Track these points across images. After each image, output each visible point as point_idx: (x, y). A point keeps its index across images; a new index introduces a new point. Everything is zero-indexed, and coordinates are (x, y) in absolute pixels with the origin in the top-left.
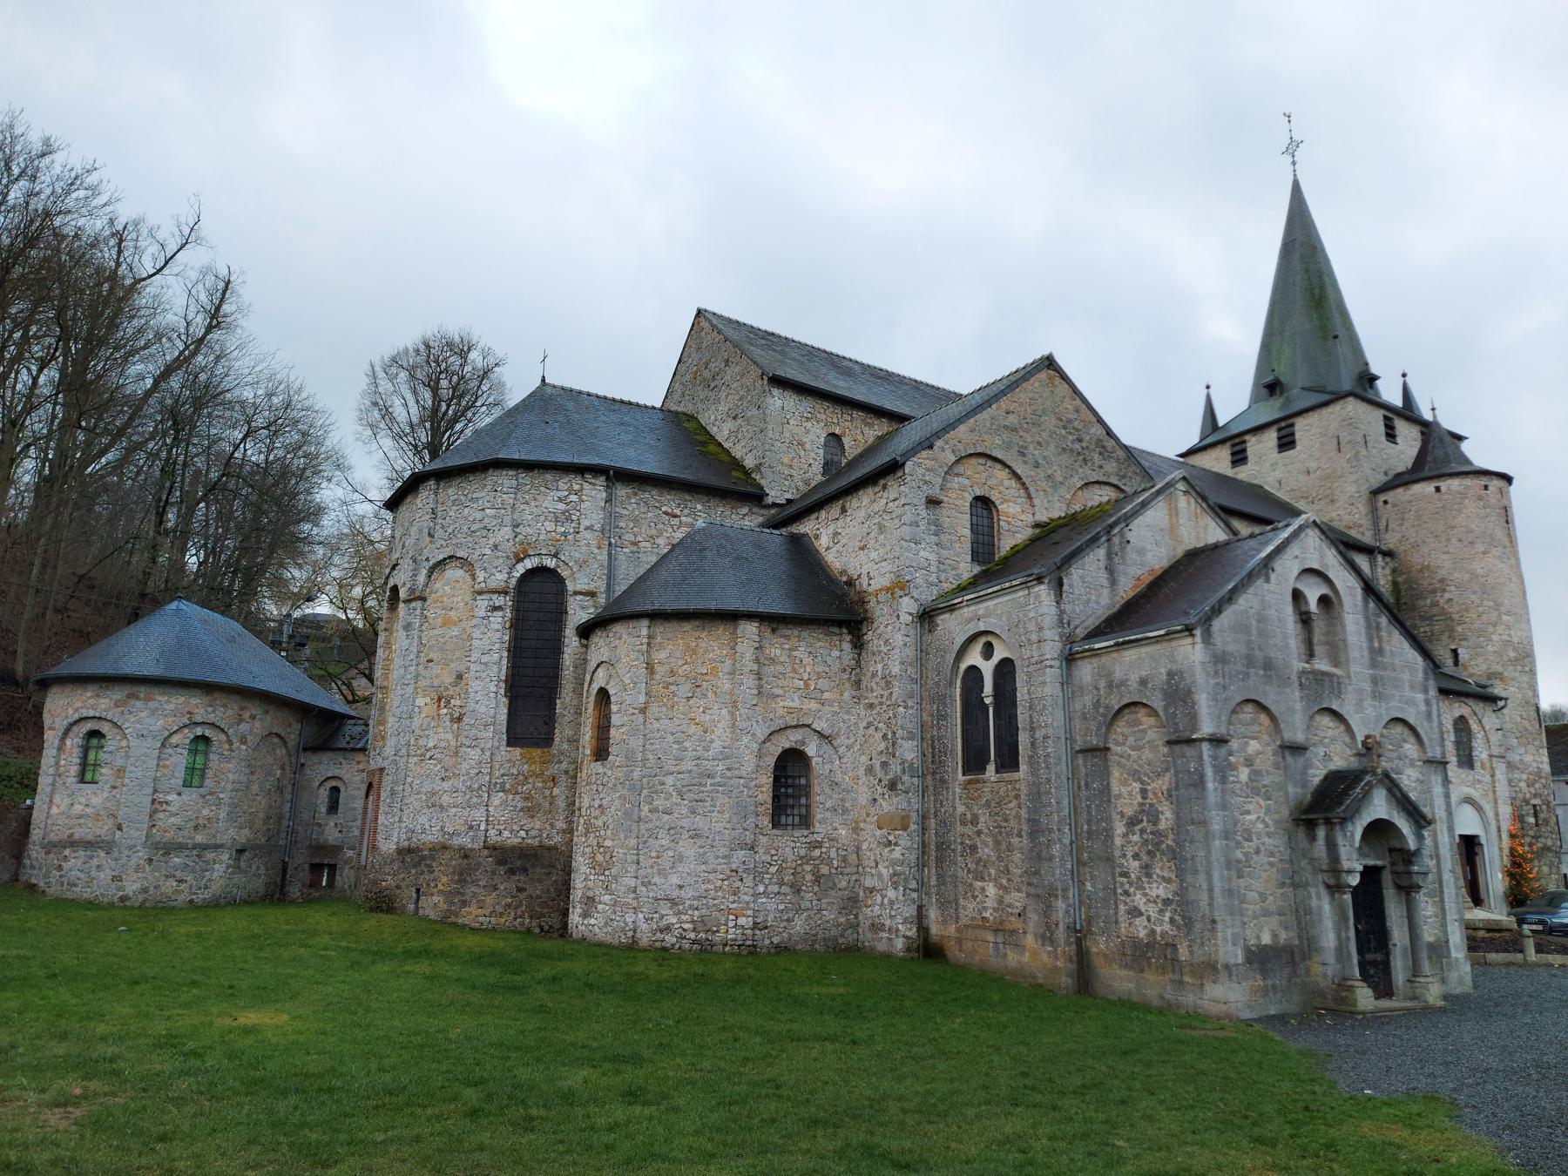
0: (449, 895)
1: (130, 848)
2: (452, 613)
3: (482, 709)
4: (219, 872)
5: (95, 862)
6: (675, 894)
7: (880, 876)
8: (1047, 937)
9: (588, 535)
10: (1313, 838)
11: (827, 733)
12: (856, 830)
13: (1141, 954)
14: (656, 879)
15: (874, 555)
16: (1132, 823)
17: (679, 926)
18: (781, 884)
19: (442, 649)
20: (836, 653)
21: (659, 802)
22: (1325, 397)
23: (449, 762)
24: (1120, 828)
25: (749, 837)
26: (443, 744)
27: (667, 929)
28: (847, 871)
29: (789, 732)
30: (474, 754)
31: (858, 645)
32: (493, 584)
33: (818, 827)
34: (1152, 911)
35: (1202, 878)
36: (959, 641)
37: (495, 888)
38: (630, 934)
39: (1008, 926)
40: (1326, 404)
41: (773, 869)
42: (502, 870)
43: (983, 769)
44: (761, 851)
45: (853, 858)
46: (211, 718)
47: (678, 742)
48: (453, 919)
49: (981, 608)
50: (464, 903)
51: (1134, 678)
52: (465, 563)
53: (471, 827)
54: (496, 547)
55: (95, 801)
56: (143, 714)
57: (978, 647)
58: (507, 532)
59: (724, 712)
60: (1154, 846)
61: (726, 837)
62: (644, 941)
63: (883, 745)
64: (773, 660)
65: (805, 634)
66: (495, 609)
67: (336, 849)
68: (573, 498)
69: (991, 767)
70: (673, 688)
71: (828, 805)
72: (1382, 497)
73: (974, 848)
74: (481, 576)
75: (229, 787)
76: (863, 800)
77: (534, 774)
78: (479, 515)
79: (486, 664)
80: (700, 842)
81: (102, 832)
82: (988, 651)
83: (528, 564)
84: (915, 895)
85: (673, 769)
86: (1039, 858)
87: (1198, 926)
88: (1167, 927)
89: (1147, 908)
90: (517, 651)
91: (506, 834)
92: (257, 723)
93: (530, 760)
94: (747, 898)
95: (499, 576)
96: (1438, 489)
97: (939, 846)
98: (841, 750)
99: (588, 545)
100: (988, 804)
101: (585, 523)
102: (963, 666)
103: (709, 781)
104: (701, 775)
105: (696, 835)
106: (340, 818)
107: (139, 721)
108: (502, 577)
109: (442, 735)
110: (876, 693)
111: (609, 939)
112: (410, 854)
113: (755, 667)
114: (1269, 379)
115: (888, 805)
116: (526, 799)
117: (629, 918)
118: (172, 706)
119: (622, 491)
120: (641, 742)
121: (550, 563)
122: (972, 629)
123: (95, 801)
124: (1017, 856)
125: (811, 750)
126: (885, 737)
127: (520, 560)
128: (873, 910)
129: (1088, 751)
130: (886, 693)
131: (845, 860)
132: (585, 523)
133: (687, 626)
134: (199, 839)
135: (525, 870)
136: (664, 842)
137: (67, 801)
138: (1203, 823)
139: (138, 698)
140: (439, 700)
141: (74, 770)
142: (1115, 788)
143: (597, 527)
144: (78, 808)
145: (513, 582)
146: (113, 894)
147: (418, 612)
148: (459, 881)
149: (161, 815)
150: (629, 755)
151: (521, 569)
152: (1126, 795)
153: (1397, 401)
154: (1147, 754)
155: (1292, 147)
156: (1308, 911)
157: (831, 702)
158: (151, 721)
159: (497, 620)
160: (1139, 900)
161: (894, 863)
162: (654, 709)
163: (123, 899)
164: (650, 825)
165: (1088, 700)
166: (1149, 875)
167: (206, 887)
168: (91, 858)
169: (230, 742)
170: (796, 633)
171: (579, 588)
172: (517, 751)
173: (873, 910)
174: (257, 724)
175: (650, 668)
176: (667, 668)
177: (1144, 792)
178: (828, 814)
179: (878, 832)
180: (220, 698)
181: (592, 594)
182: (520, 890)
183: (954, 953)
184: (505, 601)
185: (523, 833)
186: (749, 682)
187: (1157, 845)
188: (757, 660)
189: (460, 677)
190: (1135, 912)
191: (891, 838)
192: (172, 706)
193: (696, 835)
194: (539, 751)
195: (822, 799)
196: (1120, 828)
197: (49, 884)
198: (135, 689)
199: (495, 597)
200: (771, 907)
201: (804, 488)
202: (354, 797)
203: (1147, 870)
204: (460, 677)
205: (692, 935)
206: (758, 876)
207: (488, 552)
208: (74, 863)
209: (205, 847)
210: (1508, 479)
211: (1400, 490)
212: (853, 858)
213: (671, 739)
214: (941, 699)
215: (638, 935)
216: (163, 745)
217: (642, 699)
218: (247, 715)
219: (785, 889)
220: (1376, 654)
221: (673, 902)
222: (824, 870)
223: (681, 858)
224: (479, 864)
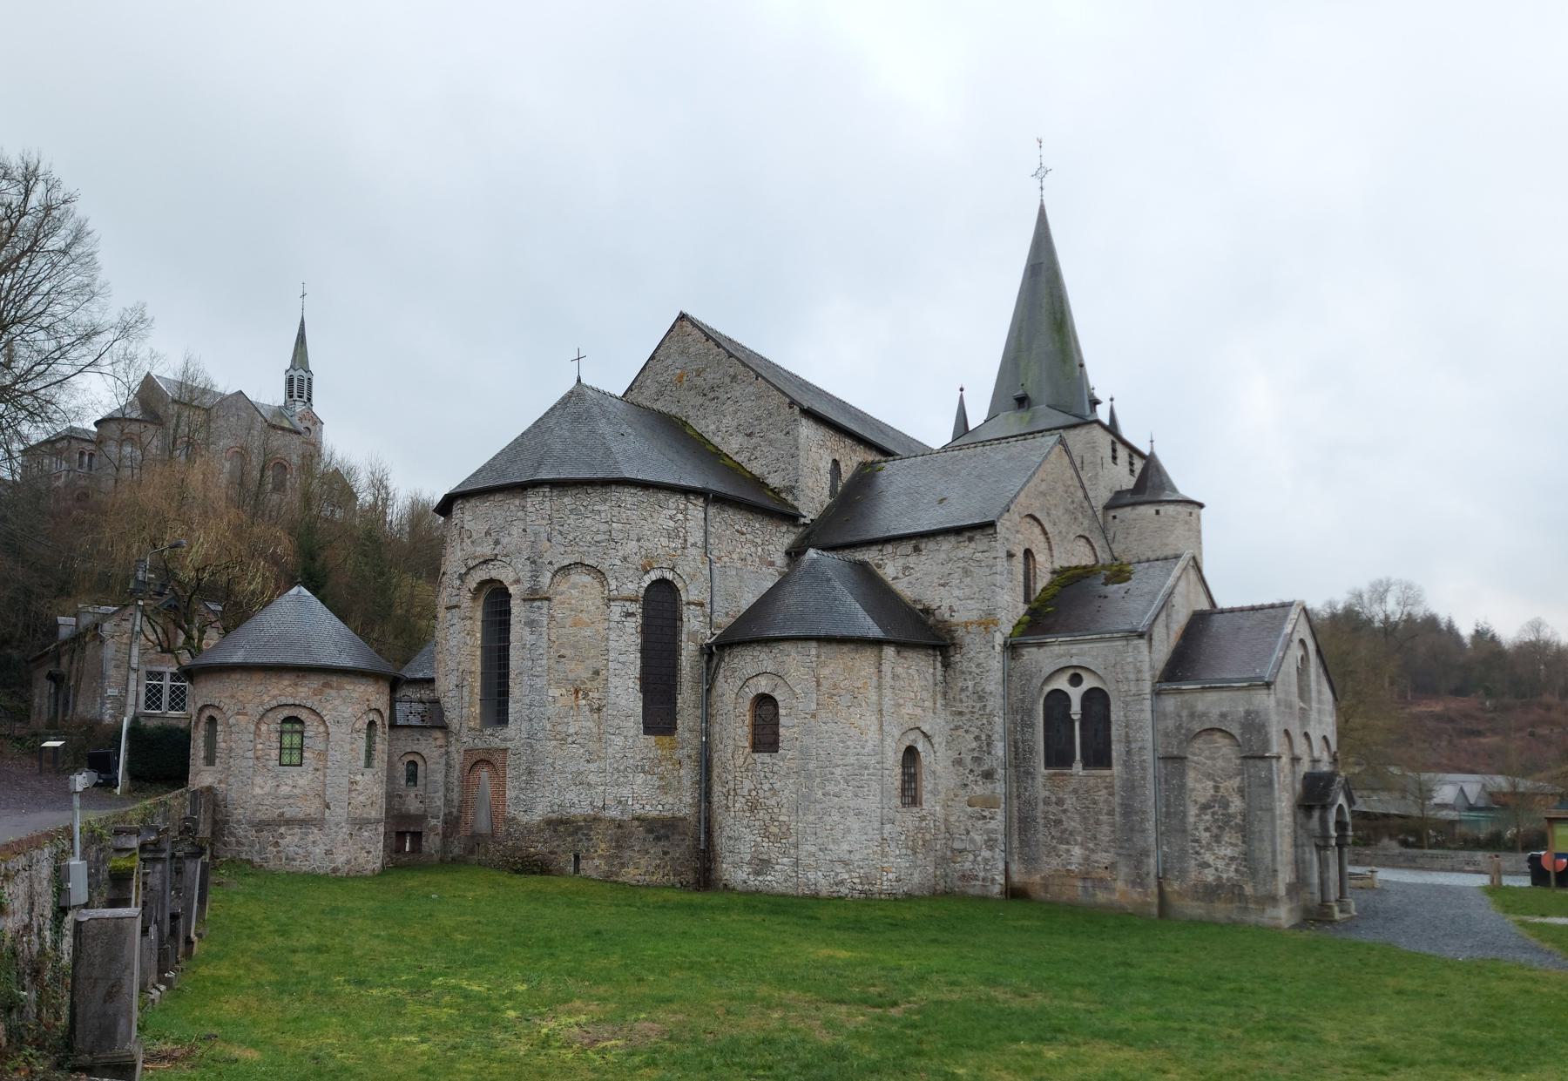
0: (609, 859)
1: (337, 824)
3: (623, 702)
8: (1138, 881)
9: (693, 551)
10: (1309, 817)
13: (1211, 892)
15: (956, 592)
16: (1205, 808)
17: (850, 880)
19: (574, 647)
21: (831, 788)
22: (1074, 420)
23: (592, 746)
24: (1193, 811)
30: (619, 740)
31: (946, 665)
32: (625, 593)
34: (1220, 864)
36: (1048, 670)
37: (647, 852)
39: (1094, 875)
40: (1074, 426)
49: (1075, 649)
50: (623, 865)
52: (599, 574)
54: (625, 559)
55: (301, 782)
57: (1066, 677)
60: (1224, 823)
66: (629, 615)
67: (421, 818)
68: (680, 516)
69: (1077, 767)
72: (1112, 513)
73: (1059, 822)
74: (613, 584)
78: (604, 527)
81: (312, 811)
82: (1076, 680)
83: (654, 575)
86: (1132, 830)
88: (1232, 874)
89: (1218, 860)
93: (662, 747)
95: (630, 586)
96: (1158, 512)
97: (1020, 820)
100: (1075, 791)
101: (691, 540)
102: (1048, 689)
104: (861, 767)
106: (420, 789)
107: (335, 709)
109: (582, 723)
111: (790, 891)
112: (560, 825)
114: (1020, 393)
118: (355, 695)
121: (669, 576)
122: (1063, 663)
124: (1106, 828)
125: (920, 748)
133: (845, 649)
137: (271, 783)
138: (1271, 810)
140: (577, 692)
142: (1190, 783)
144: (285, 790)
145: (642, 591)
146: (327, 867)
147: (545, 611)
148: (617, 847)
152: (1199, 788)
155: (1041, 173)
156: (1304, 862)
159: (634, 624)
160: (1208, 857)
162: (822, 714)
163: (335, 870)
166: (1218, 842)
168: (307, 834)
171: (692, 598)
172: (652, 739)
177: (1217, 788)
181: (701, 605)
182: (665, 853)
184: (635, 608)
187: (1227, 823)
189: (597, 673)
192: (355, 695)
196: (1193, 811)
197: (266, 860)
201: (820, 510)
202: (434, 771)
204: (597, 673)
208: (291, 840)
210: (1201, 506)
211: (1128, 509)
214: (1030, 712)
221: (846, 863)
223: (849, 830)
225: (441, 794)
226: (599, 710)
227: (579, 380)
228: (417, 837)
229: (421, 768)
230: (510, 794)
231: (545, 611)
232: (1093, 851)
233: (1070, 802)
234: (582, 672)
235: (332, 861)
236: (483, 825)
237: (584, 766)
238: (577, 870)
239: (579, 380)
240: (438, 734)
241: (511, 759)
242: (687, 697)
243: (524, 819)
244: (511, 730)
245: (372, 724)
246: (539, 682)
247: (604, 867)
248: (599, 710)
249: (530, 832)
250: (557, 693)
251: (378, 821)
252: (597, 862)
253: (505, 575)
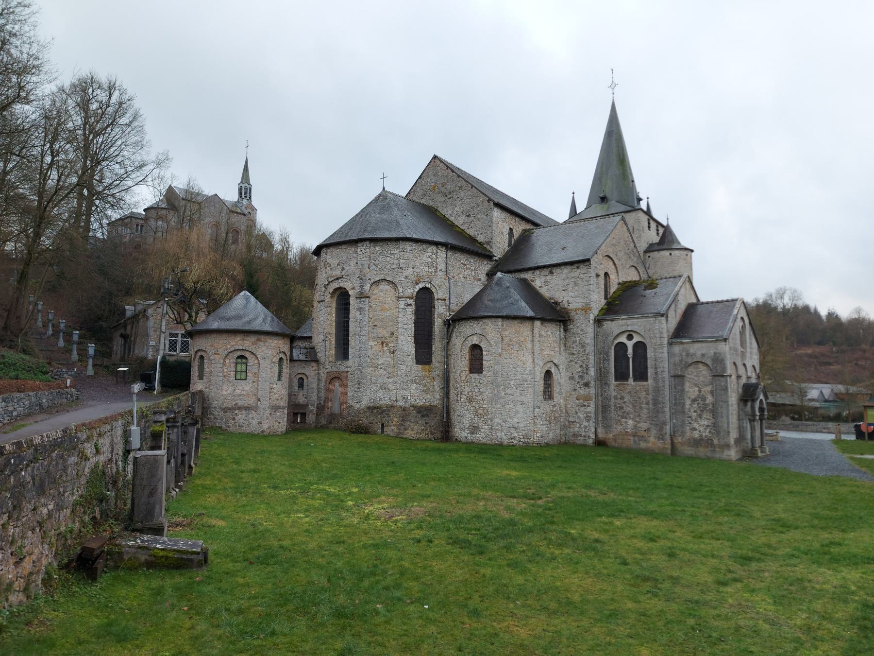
0: (399, 426)
2: (386, 305)
5: (251, 416)
10: (746, 405)
13: (696, 443)
15: (571, 294)
16: (694, 401)
17: (518, 437)
19: (381, 321)
21: (509, 391)
22: (629, 209)
24: (688, 402)
30: (403, 367)
31: (566, 330)
32: (407, 294)
35: (725, 419)
43: (627, 379)
49: (630, 322)
50: (405, 429)
51: (699, 353)
55: (246, 388)
60: (703, 408)
62: (505, 443)
66: (408, 305)
67: (306, 406)
68: (434, 256)
69: (631, 381)
72: (648, 254)
73: (622, 408)
74: (401, 290)
81: (251, 402)
82: (630, 337)
83: (421, 286)
86: (658, 412)
87: (722, 434)
89: (701, 427)
93: (425, 371)
100: (630, 392)
101: (439, 268)
102: (616, 342)
105: (522, 404)
107: (263, 352)
109: (387, 358)
110: (576, 349)
111: (488, 442)
112: (374, 409)
114: (602, 195)
117: (499, 434)
121: (428, 286)
122: (624, 329)
123: (246, 388)
126: (581, 366)
129: (676, 376)
133: (516, 322)
135: (427, 415)
137: (231, 388)
140: (383, 343)
141: (233, 374)
142: (687, 388)
144: (238, 392)
145: (415, 293)
147: (367, 303)
150: (496, 374)
151: (417, 288)
152: (691, 391)
153: (645, 209)
154: (702, 379)
155: (613, 86)
158: (266, 351)
160: (696, 425)
162: (504, 355)
163: (263, 432)
165: (677, 359)
166: (701, 418)
171: (440, 297)
177: (700, 391)
181: (444, 300)
182: (427, 423)
183: (611, 443)
187: (705, 408)
190: (694, 429)
193: (522, 404)
196: (688, 402)
201: (503, 253)
203: (700, 416)
204: (393, 334)
208: (241, 416)
210: (692, 251)
220: (751, 343)
221: (516, 428)
223: (517, 412)
225: (315, 394)
226: (394, 352)
228: (303, 415)
229: (305, 381)
230: (350, 394)
231: (367, 303)
232: (638, 422)
233: (627, 398)
234: (385, 334)
235: (261, 427)
236: (336, 409)
237: (386, 380)
238: (383, 431)
240: (314, 364)
241: (350, 377)
242: (437, 346)
243: (357, 406)
244: (350, 362)
245: (281, 359)
246: (364, 339)
247: (396, 430)
248: (394, 352)
249: (360, 413)
250: (372, 344)
251: (284, 408)
252: (393, 428)
253: (347, 285)
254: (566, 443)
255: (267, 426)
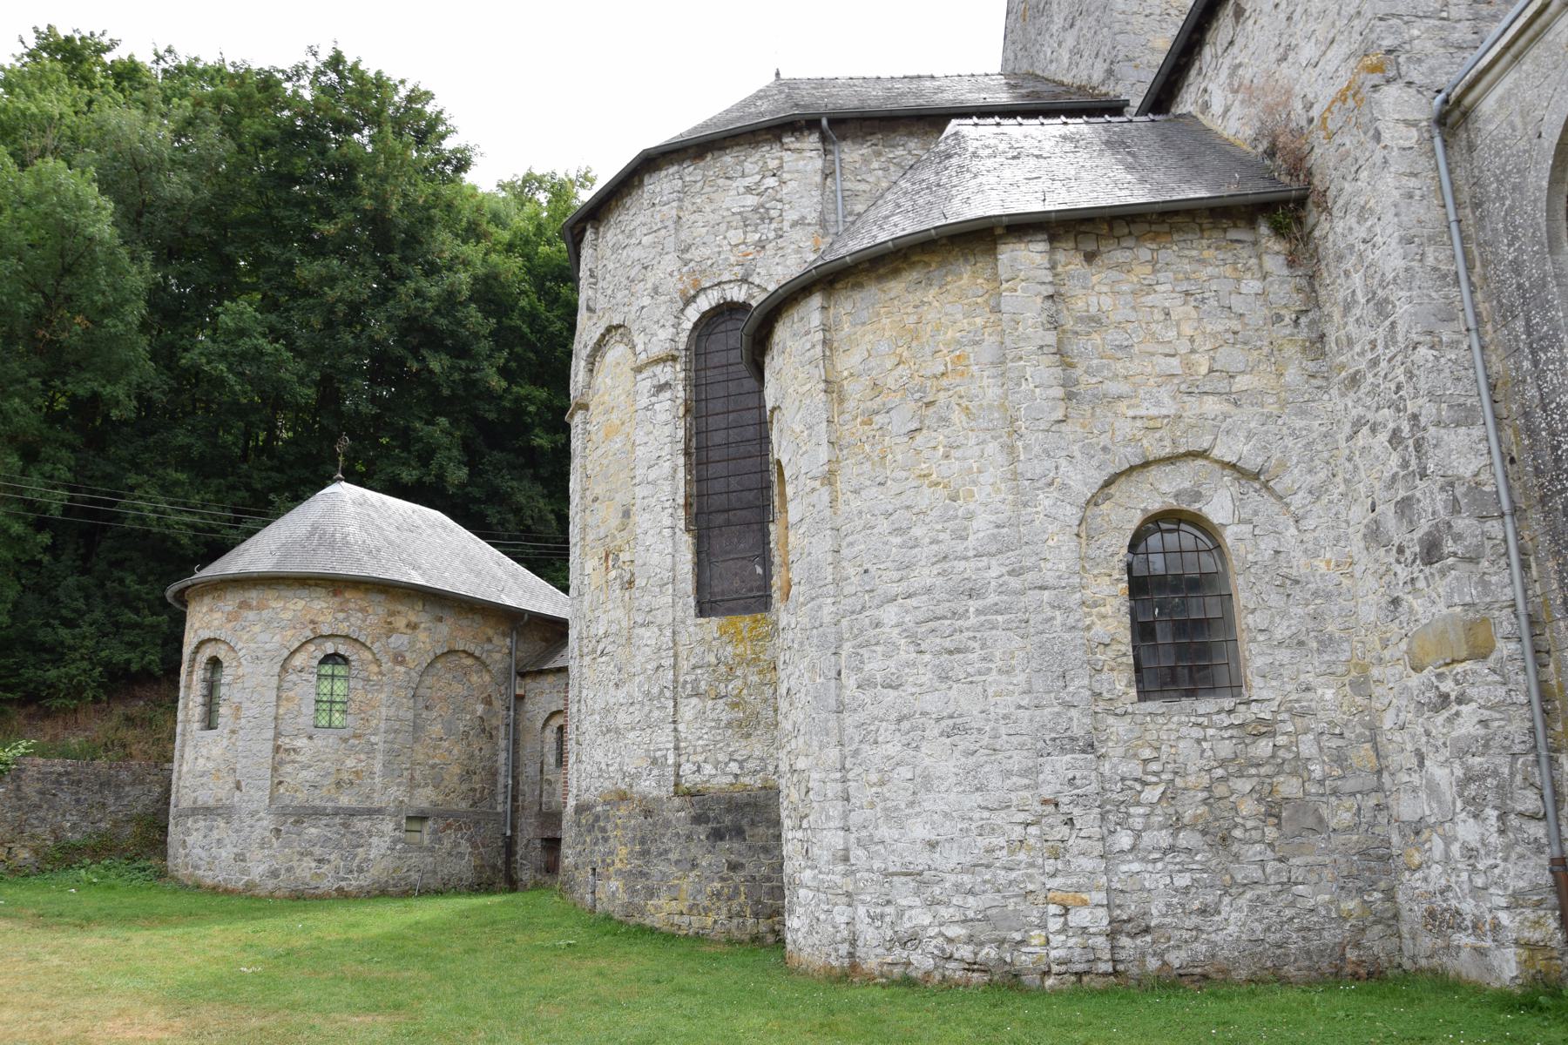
0: (630, 876)
1: (252, 814)
4: (380, 848)
5: (215, 835)
6: (922, 860)
7: (1433, 789)
9: (798, 234)
11: (1252, 464)
12: (1361, 685)
14: (884, 832)
18: (1176, 826)
20: (1252, 285)
21: (875, 665)
23: (621, 654)
25: (1079, 723)
26: (614, 628)
27: (911, 940)
28: (1350, 784)
29: (1154, 472)
30: (648, 636)
32: (656, 350)
33: (1257, 687)
38: (844, 949)
41: (1151, 794)
42: (702, 831)
44: (1115, 751)
45: (1362, 755)
46: (343, 628)
47: (898, 531)
48: (637, 919)
50: (651, 893)
53: (654, 761)
56: (257, 629)
58: (670, 262)
59: (992, 447)
61: (1024, 726)
62: (871, 961)
63: (1394, 460)
64: (1095, 321)
65: (1168, 254)
68: (771, 182)
70: (879, 419)
71: (1281, 632)
74: (639, 340)
75: (382, 725)
76: (1370, 609)
77: (743, 661)
79: (654, 483)
80: (965, 743)
81: (222, 794)
83: (705, 303)
84: (1537, 830)
85: (895, 589)
90: (698, 453)
91: (708, 769)
92: (427, 635)
94: (1088, 864)
98: (1297, 501)
99: (799, 250)
103: (973, 605)
104: (955, 593)
105: (956, 728)
107: (253, 639)
108: (665, 334)
110: (1351, 329)
113: (1051, 338)
115: (1437, 600)
116: (735, 705)
119: (852, 154)
120: (828, 544)
125: (1217, 509)
126: (1395, 438)
127: (689, 301)
128: (1427, 878)
130: (1381, 333)
131: (1340, 759)
132: (792, 216)
134: (345, 800)
135: (739, 832)
136: (891, 750)
139: (250, 607)
143: (812, 217)
145: (683, 338)
148: (645, 853)
149: (288, 768)
151: (693, 314)
157: (1256, 397)
161: (1462, 752)
162: (850, 472)
163: (249, 886)
164: (861, 716)
167: (360, 870)
169: (377, 662)
170: (1144, 253)
172: (713, 624)
173: (1427, 878)
174: (422, 636)
175: (831, 386)
176: (865, 381)
178: (1283, 655)
179: (1415, 680)
180: (354, 599)
182: (734, 867)
184: (674, 373)
185: (734, 767)
186: (1040, 374)
188: (1054, 324)
191: (1447, 686)
192: (288, 615)
193: (956, 728)
194: (748, 619)
195: (1261, 626)
198: (247, 595)
199: (658, 369)
200: (1156, 885)
205: (966, 952)
206: (1111, 811)
207: (646, 301)
209: (352, 813)
212: (1362, 755)
213: (884, 526)
215: (861, 952)
216: (284, 668)
217: (824, 454)
218: (400, 622)
219: (1185, 839)
222: (1289, 787)
223: (927, 782)
224: (667, 824)
227: (778, 74)
235: (244, 872)
239: (778, 74)
247: (623, 897)
254: (1375, 978)
255: (263, 868)
